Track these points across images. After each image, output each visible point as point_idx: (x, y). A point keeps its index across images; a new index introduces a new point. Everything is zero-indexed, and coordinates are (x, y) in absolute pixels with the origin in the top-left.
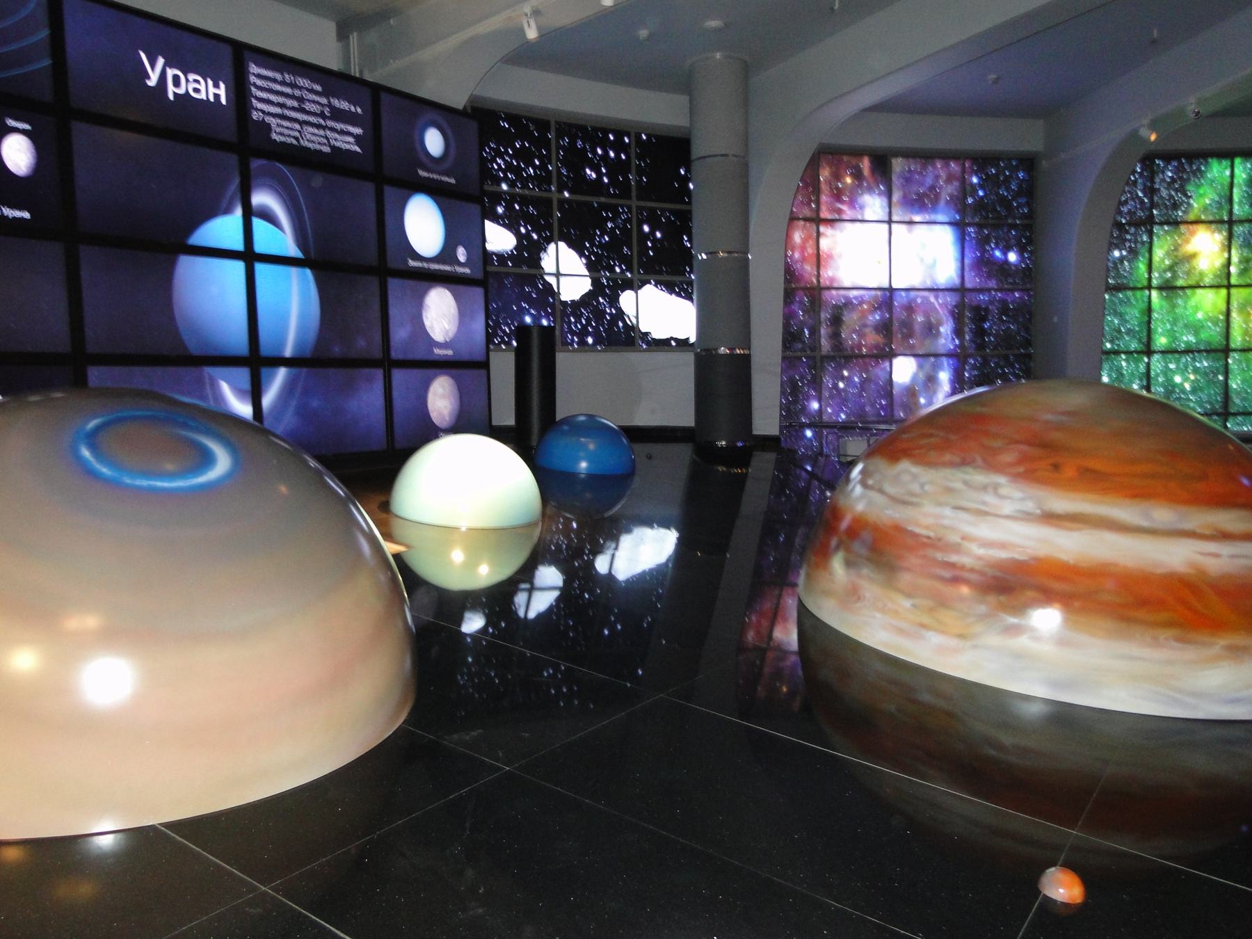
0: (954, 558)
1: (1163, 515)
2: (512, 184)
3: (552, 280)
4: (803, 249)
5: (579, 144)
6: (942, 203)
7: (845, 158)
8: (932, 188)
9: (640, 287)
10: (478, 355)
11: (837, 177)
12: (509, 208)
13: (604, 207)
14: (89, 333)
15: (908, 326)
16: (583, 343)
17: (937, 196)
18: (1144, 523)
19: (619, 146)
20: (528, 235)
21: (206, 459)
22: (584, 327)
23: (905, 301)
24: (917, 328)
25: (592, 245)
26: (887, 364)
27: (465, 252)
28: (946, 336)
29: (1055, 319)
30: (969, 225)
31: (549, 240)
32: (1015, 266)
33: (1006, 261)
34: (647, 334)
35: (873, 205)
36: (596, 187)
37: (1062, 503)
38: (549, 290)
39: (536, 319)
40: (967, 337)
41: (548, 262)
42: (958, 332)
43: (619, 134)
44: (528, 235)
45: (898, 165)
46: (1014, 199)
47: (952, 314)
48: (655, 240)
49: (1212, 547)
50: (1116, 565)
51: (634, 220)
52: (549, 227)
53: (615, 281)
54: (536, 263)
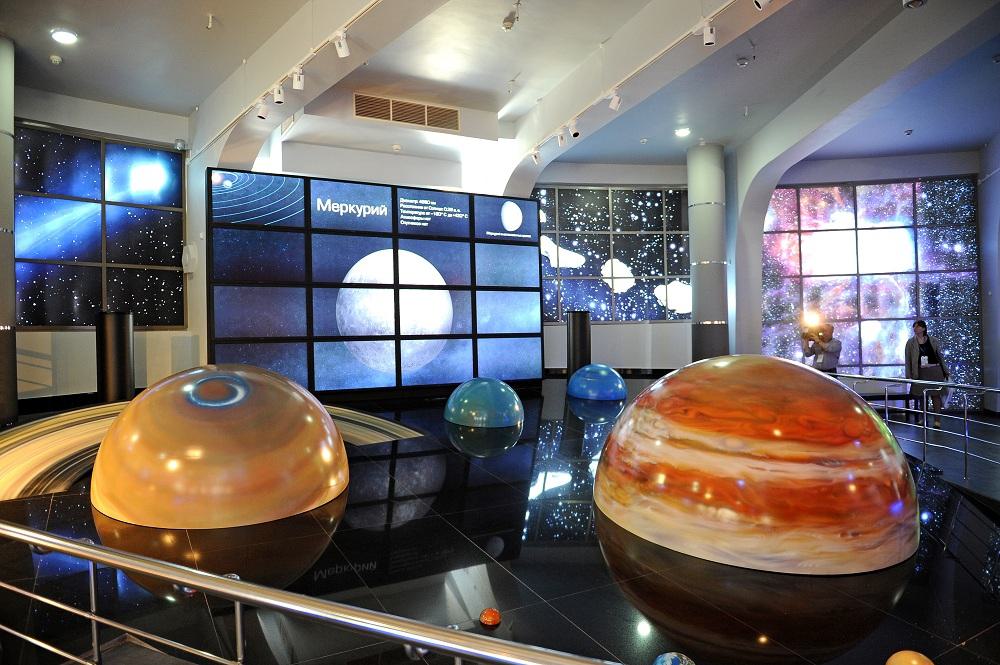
0: (628, 461)
1: (734, 443)
2: (583, 229)
3: (609, 282)
4: (789, 251)
5: (627, 200)
6: (898, 213)
7: (820, 189)
8: (890, 204)
9: (669, 283)
10: (539, 331)
11: (814, 203)
12: (581, 241)
13: (642, 236)
14: (315, 327)
15: (873, 302)
16: (629, 318)
17: (894, 210)
18: (721, 447)
19: (654, 198)
20: (593, 257)
21: (234, 394)
22: (630, 308)
23: (870, 283)
24: (881, 301)
25: (636, 259)
26: (857, 325)
27: (337, 306)
28: (905, 307)
29: (990, 293)
30: (920, 227)
31: (607, 258)
32: (961, 253)
33: (953, 251)
34: (673, 311)
35: (842, 217)
36: (639, 225)
37: (681, 432)
38: (606, 287)
39: (598, 305)
40: (922, 306)
41: (606, 270)
42: (915, 303)
43: (654, 193)
44: (593, 257)
45: (861, 190)
46: (957, 206)
47: (909, 290)
48: (679, 253)
49: (760, 464)
50: (698, 471)
51: (665, 242)
52: (608, 251)
53: (651, 280)
54: (598, 273)
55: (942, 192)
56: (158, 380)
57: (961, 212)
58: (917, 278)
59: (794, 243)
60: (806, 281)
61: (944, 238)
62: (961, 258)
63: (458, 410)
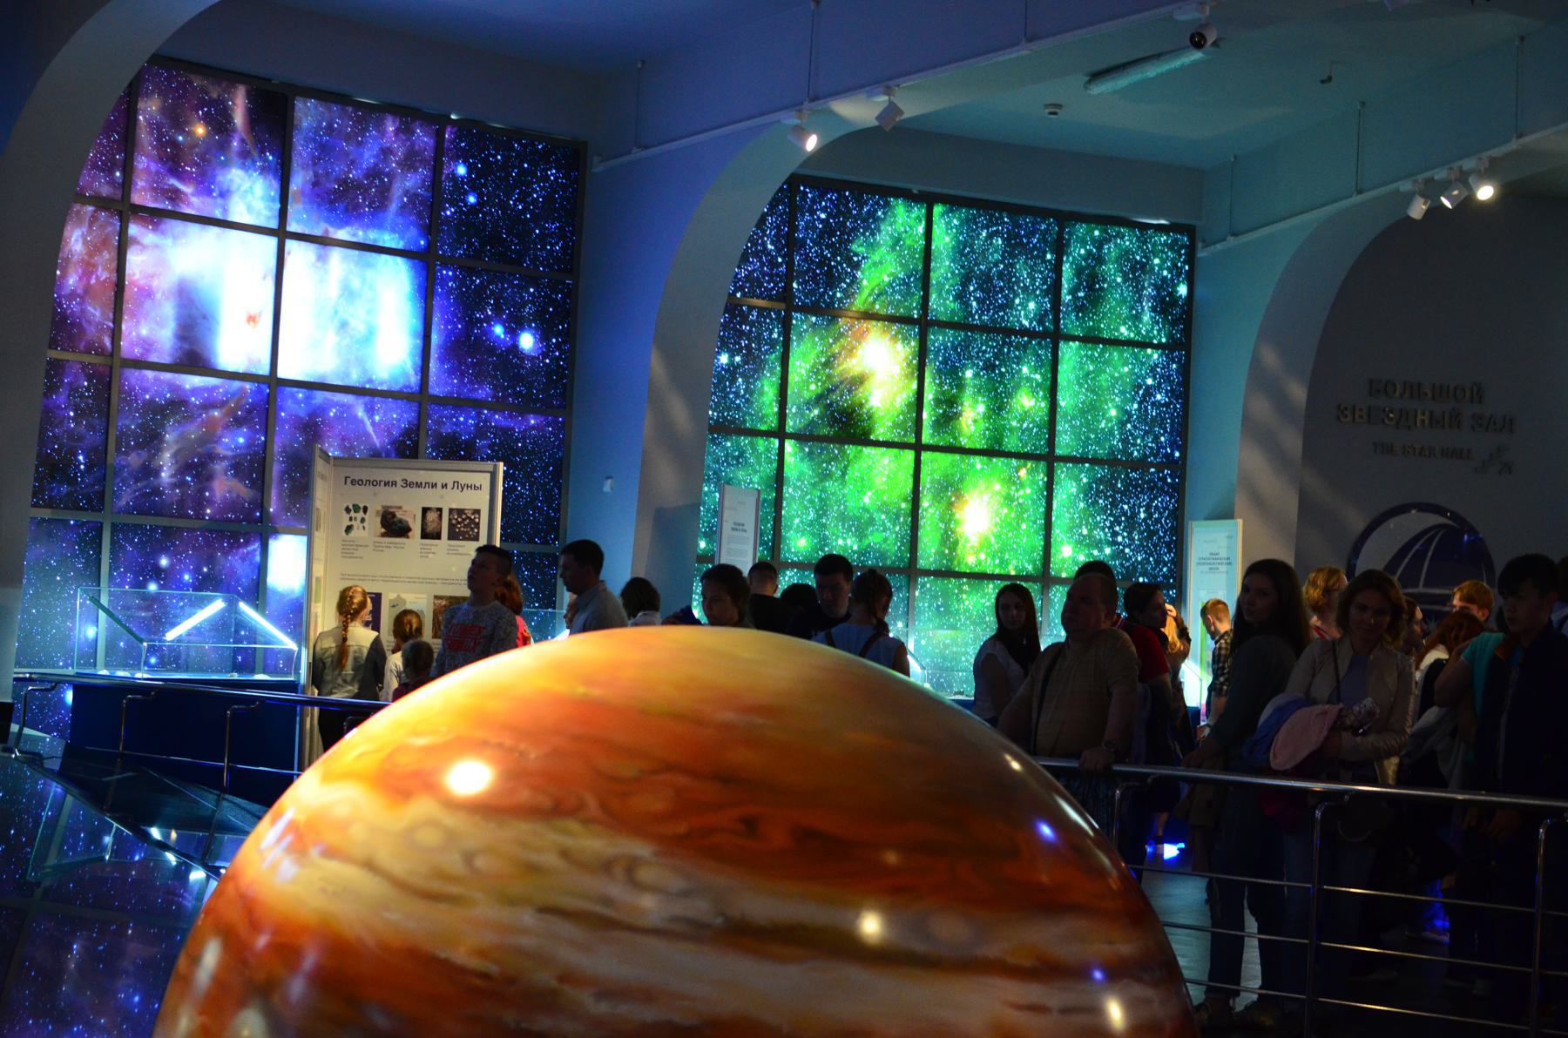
4: (88, 269)
6: (393, 207)
8: (374, 173)
23: (302, 411)
55: (505, 166)
56: (464, 556)
57: (542, 238)
58: (768, 434)
59: (105, 243)
60: (436, 389)
61: (497, 309)
62: (533, 371)
63: (12, 772)
